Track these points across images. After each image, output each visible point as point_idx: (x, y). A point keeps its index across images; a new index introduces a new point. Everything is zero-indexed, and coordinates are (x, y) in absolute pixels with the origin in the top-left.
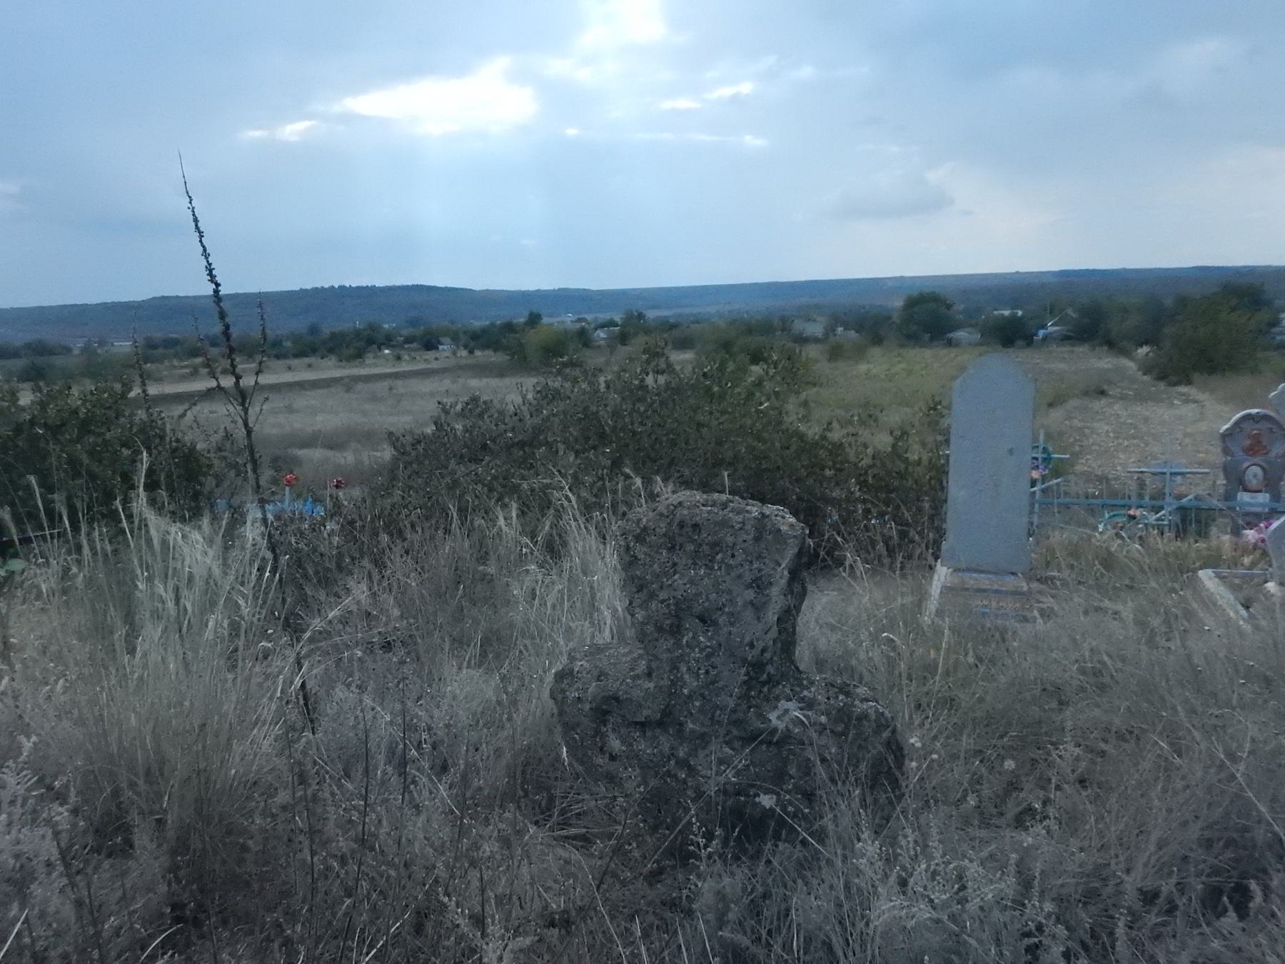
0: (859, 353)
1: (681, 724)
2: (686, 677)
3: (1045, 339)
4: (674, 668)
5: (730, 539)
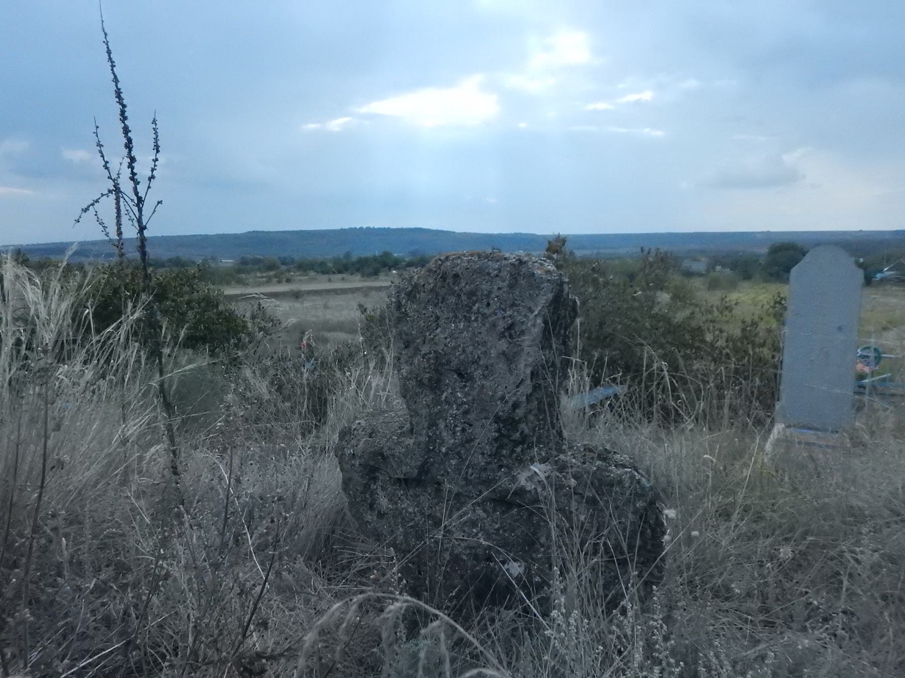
0: (732, 285)
1: (439, 484)
2: (444, 434)
3: (882, 280)
4: (433, 424)
5: (485, 287)
